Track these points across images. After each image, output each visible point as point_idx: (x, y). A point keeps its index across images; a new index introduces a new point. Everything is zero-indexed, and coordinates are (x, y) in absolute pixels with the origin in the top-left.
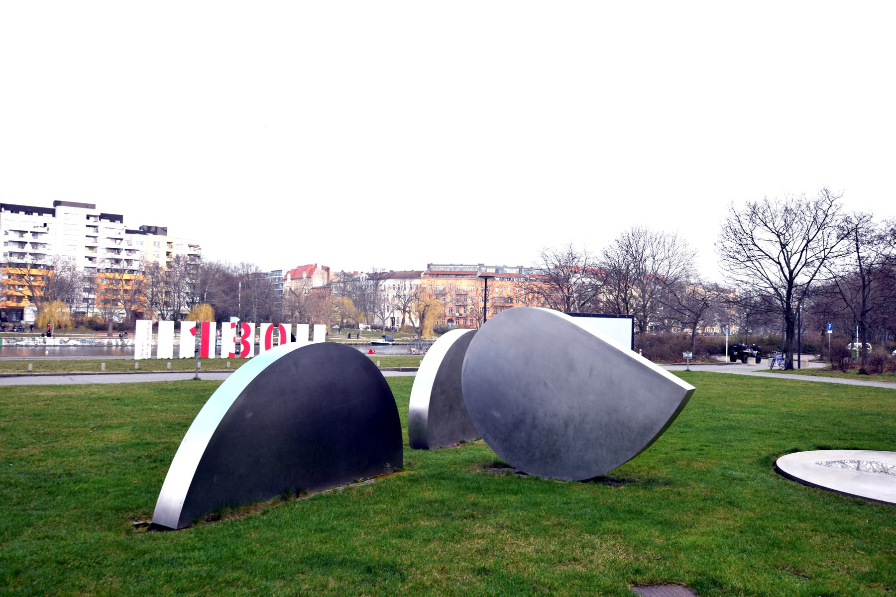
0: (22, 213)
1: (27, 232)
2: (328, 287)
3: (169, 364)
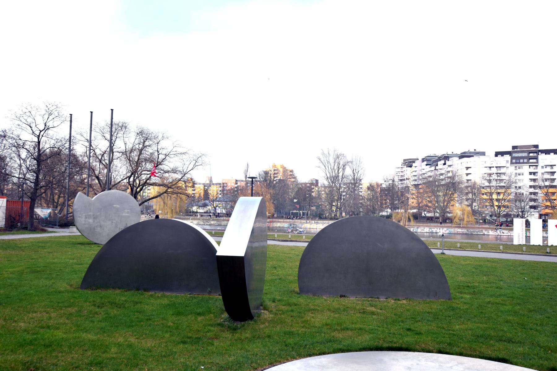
0: (552, 154)
1: (494, 167)
2: (298, 190)
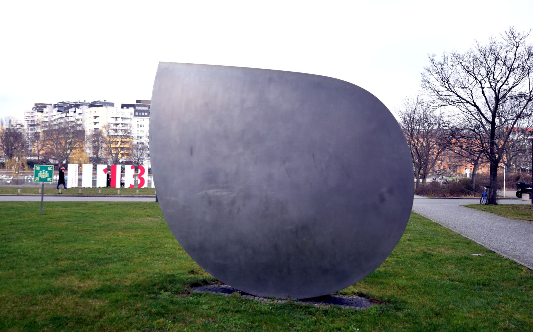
3: (80, 190)
